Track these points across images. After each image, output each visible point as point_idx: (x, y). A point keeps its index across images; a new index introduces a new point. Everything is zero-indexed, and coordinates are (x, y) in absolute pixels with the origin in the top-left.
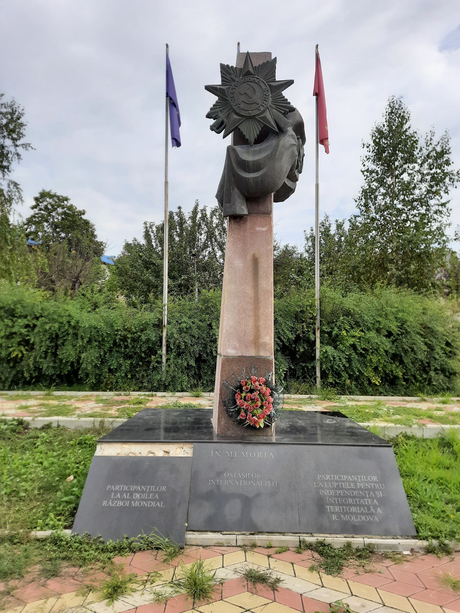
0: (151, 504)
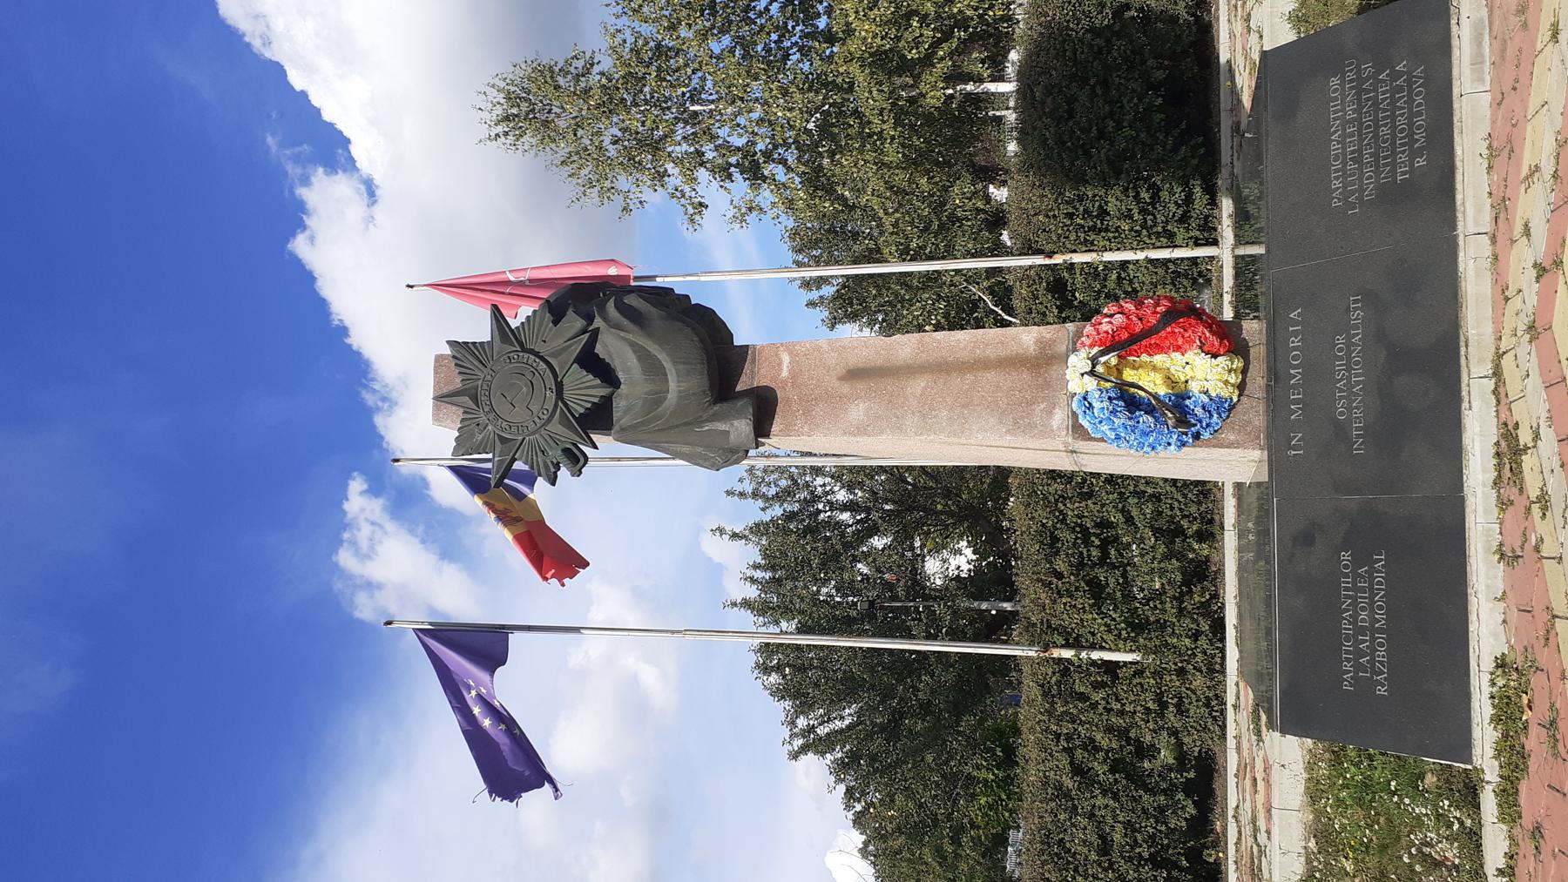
0: (1379, 583)
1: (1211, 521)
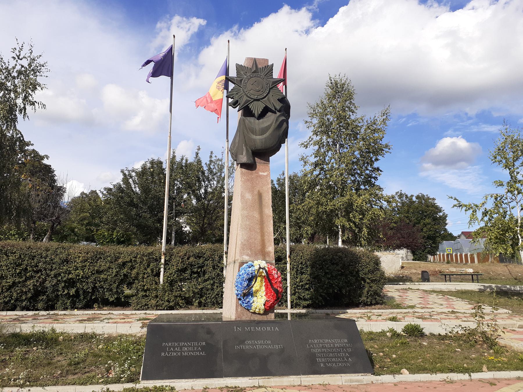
1: (205, 306)
